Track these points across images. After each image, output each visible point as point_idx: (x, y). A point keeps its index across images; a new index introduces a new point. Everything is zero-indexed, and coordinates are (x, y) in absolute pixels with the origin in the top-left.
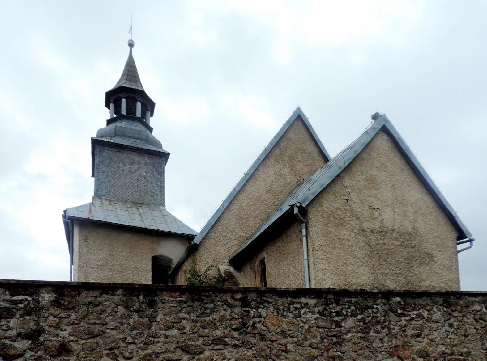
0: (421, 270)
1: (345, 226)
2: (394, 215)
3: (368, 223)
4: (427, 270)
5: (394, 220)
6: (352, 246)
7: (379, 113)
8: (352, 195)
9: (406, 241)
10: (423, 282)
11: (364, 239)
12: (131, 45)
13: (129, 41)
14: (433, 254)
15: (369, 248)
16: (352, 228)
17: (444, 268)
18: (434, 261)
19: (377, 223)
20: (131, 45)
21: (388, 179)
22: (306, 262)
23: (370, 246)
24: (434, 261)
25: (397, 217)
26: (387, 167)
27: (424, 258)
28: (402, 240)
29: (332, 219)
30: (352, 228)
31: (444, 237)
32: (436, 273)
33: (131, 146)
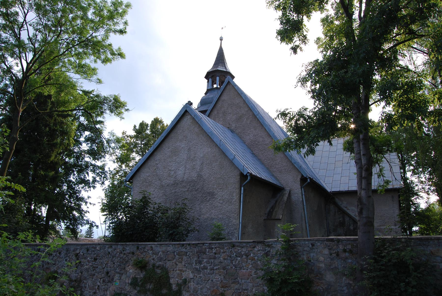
0: (202, 206)
1: (152, 186)
2: (185, 170)
3: (166, 181)
4: (207, 206)
5: (185, 173)
6: (155, 197)
7: (158, 119)
8: (159, 166)
9: (191, 187)
10: (202, 216)
11: (162, 192)
12: (221, 39)
13: (220, 37)
14: (214, 192)
15: (165, 197)
16: (156, 186)
17: (224, 202)
18: (214, 198)
19: (172, 179)
20: (221, 39)
21: (186, 146)
22: (305, 204)
23: (166, 196)
24: (214, 198)
25: (187, 171)
26: (187, 137)
27: (205, 197)
28: (188, 187)
29: (145, 183)
30: (156, 186)
31: (226, 177)
32: (215, 207)
33: (254, 106)
